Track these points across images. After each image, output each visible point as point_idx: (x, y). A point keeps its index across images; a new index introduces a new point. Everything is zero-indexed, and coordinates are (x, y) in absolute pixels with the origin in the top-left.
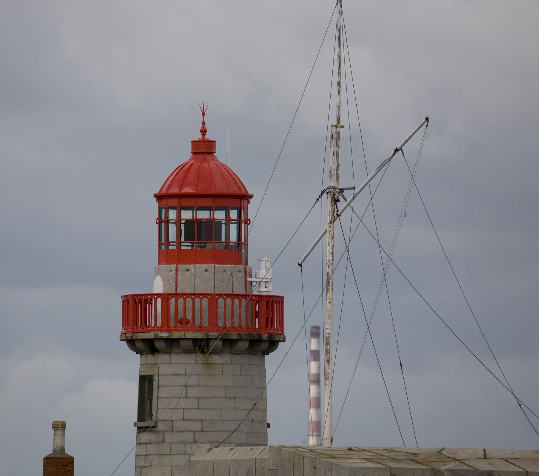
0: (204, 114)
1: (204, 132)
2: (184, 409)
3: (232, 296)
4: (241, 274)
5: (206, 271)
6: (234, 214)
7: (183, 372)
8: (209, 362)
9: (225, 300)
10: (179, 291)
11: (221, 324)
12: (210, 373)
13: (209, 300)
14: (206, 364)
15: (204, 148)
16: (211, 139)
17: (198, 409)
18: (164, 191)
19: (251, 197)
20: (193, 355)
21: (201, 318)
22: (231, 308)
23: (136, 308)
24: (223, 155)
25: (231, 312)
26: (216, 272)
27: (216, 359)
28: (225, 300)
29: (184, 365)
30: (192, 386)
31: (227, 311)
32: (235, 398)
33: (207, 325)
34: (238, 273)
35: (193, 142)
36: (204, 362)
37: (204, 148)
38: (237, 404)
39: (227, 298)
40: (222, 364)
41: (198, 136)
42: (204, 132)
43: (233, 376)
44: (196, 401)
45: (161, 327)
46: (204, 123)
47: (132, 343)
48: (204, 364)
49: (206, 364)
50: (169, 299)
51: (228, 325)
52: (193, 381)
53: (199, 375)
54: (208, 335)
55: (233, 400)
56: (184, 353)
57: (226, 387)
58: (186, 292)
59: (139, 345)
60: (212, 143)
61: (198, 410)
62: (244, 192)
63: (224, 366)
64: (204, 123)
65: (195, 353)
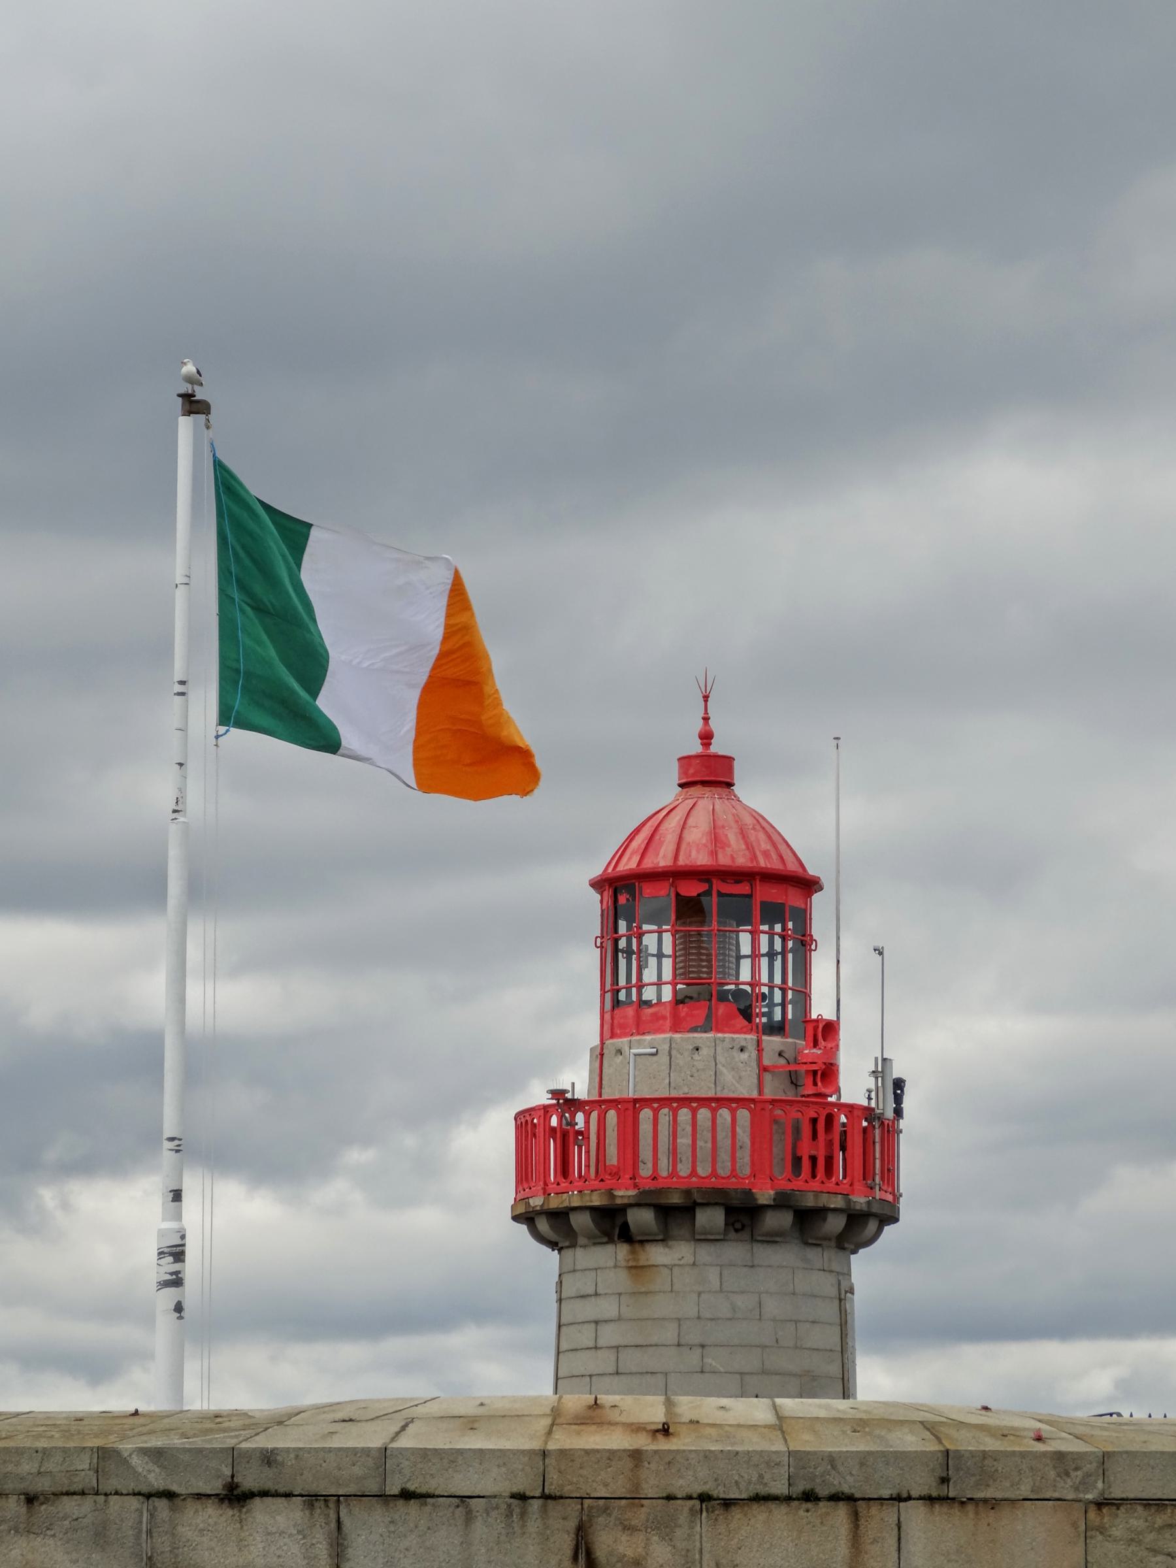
0: (706, 698)
1: (706, 737)
2: (590, 1376)
3: (716, 1103)
4: (744, 1056)
6: (778, 928)
7: (591, 1291)
8: (641, 1264)
9: (694, 1112)
10: (605, 1097)
11: (645, 1171)
12: (643, 1290)
14: (637, 1270)
15: (709, 773)
16: (722, 752)
17: (617, 1373)
18: (629, 864)
19: (810, 885)
20: (610, 1248)
21: (674, 1151)
22: (710, 1135)
23: (547, 1136)
24: (753, 793)
25: (709, 1145)
26: (674, 1052)
27: (657, 1254)
28: (694, 1112)
29: (593, 1273)
30: (606, 1321)
31: (699, 1143)
32: (703, 1346)
33: (747, 1171)
34: (736, 1053)
35: (679, 759)
36: (631, 1264)
38: (708, 1360)
40: (671, 1268)
41: (696, 748)
42: (706, 737)
43: (699, 1294)
44: (612, 1355)
46: (706, 719)
47: (526, 1217)
48: (631, 1267)
51: (684, 1170)
52: (607, 1308)
53: (620, 1294)
54: (613, 1197)
55: (699, 1350)
56: (595, 1244)
57: (679, 1320)
58: (696, 1095)
59: (543, 1225)
60: (727, 762)
61: (616, 1378)
62: (792, 866)
63: (676, 1270)
64: (706, 719)
65: (611, 1241)
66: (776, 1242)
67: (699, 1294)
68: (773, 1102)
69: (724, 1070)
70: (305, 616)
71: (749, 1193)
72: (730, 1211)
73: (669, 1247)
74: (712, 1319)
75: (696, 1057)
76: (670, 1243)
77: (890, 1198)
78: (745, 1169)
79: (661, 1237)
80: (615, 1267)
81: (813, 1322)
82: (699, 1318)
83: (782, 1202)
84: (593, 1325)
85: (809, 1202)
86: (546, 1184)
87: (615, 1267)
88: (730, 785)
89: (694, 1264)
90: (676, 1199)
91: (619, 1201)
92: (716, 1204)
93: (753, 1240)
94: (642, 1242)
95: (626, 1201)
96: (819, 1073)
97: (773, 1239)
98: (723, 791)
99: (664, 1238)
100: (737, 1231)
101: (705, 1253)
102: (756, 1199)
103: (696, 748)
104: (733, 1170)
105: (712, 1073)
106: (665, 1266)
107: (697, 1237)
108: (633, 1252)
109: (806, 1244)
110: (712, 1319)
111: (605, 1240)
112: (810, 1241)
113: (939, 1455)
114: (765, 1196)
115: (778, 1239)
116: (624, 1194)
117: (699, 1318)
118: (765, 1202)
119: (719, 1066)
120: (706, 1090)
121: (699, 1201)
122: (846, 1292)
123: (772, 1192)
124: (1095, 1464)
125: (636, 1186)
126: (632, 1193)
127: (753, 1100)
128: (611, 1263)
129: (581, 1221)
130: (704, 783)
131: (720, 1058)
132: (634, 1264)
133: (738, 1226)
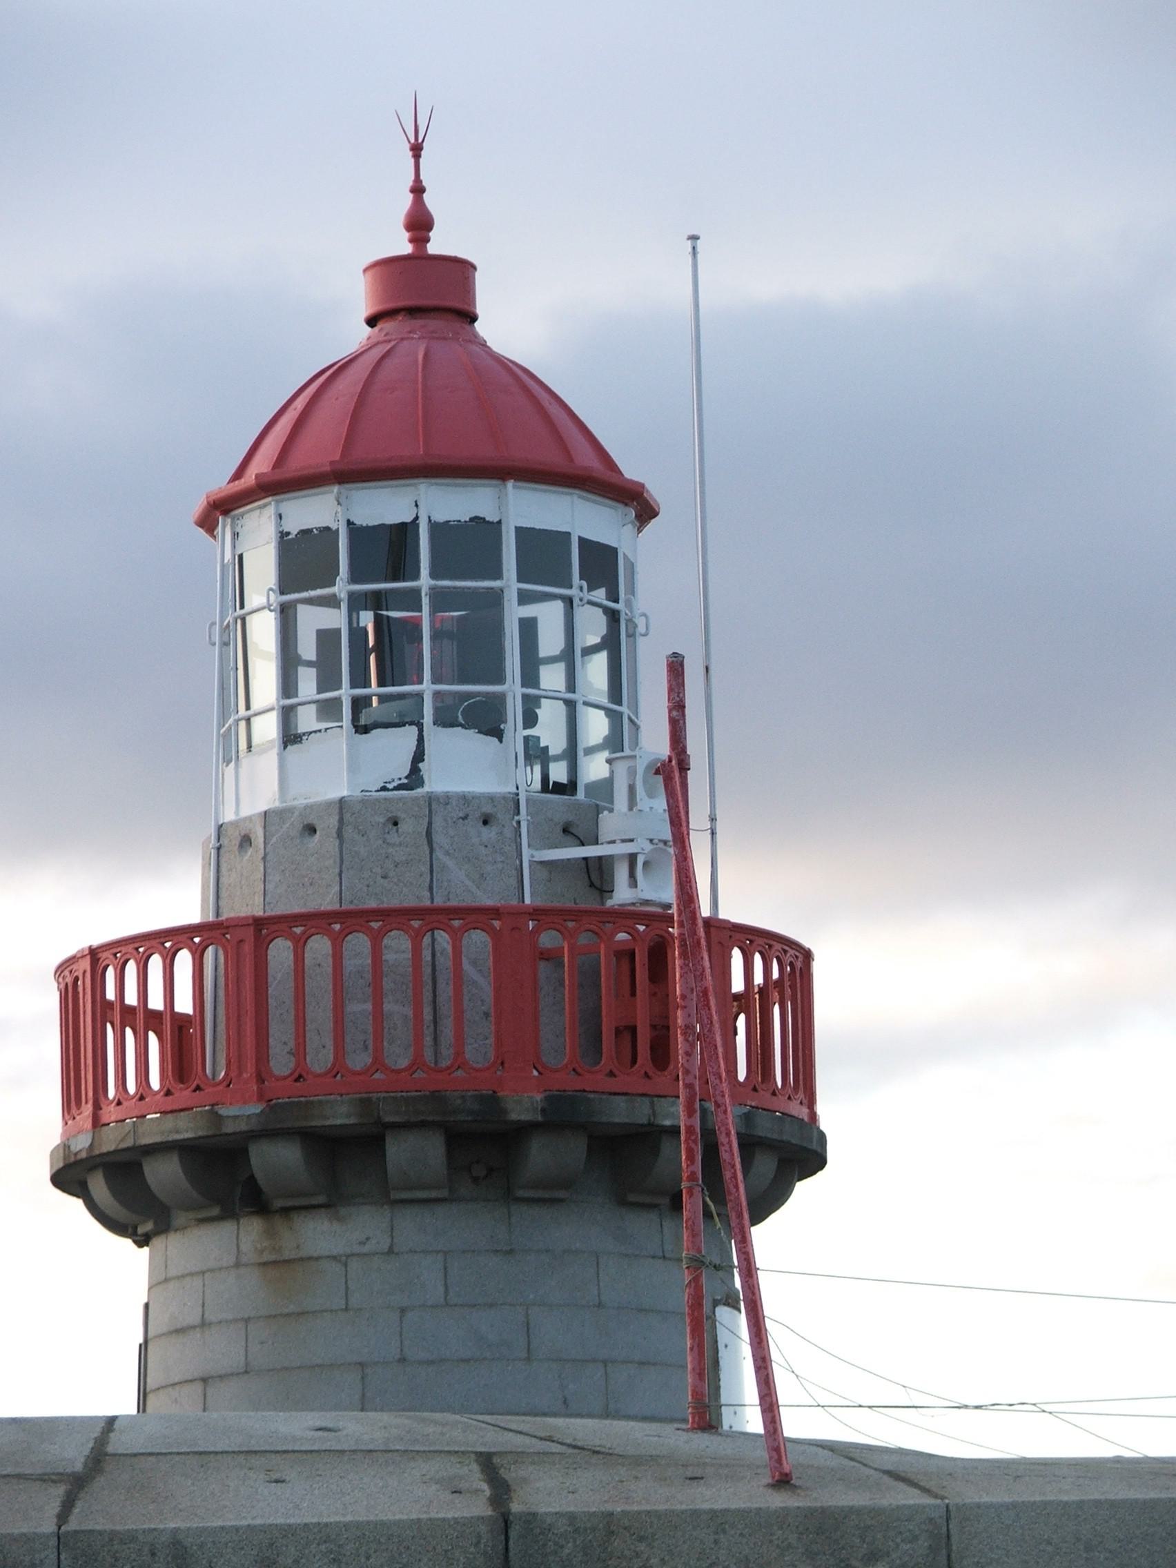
0: (417, 150)
1: (419, 224)
4: (489, 833)
5: (485, 823)
8: (287, 1255)
11: (281, 1064)
12: (292, 1308)
13: (495, 935)
14: (278, 1266)
15: (426, 291)
24: (510, 323)
26: (348, 832)
27: (318, 1235)
30: (221, 1377)
36: (267, 1257)
37: (426, 291)
39: (466, 929)
40: (342, 1260)
41: (402, 246)
42: (419, 224)
45: (228, 1081)
46: (418, 190)
48: (264, 1264)
49: (275, 1263)
50: (261, 946)
54: (216, 1118)
57: (362, 1365)
59: (98, 1185)
63: (354, 1265)
64: (418, 190)
65: (229, 1214)
66: (561, 1201)
67: (403, 1311)
68: (536, 913)
69: (450, 863)
70: (313, 593)
71: (492, 1103)
72: (460, 1139)
73: (340, 1219)
74: (431, 1362)
75: (393, 838)
76: (343, 1211)
77: (803, 1113)
78: (480, 1047)
79: (321, 1199)
80: (238, 1265)
81: (641, 1363)
82: (403, 1360)
83: (562, 1115)
84: (199, 1387)
85: (620, 1112)
86: (97, 1107)
87: (238, 1265)
88: (473, 319)
89: (391, 1251)
90: (340, 1115)
91: (229, 1128)
92: (422, 1125)
93: (509, 1196)
94: (286, 1211)
95: (243, 1127)
96: (640, 861)
97: (554, 1193)
98: (457, 324)
99: (332, 1198)
100: (476, 1180)
101: (412, 1227)
102: (504, 1112)
103: (402, 246)
104: (459, 1053)
105: (425, 869)
106: (334, 1258)
107: (395, 1195)
108: (270, 1234)
109: (623, 1202)
110: (431, 1362)
111: (216, 1211)
112: (521, 1193)
113: (483, 1529)
114: (523, 1104)
115: (561, 1194)
116: (242, 1112)
117: (403, 1360)
118: (525, 1117)
119: (438, 854)
120: (411, 895)
121: (389, 1119)
122: (716, 1303)
123: (539, 1097)
124: (923, 1543)
125: (260, 1097)
126: (255, 1109)
127: (495, 912)
128: (229, 1259)
129: (164, 1174)
130: (413, 311)
131: (438, 838)
132: (273, 1257)
133: (479, 1171)
